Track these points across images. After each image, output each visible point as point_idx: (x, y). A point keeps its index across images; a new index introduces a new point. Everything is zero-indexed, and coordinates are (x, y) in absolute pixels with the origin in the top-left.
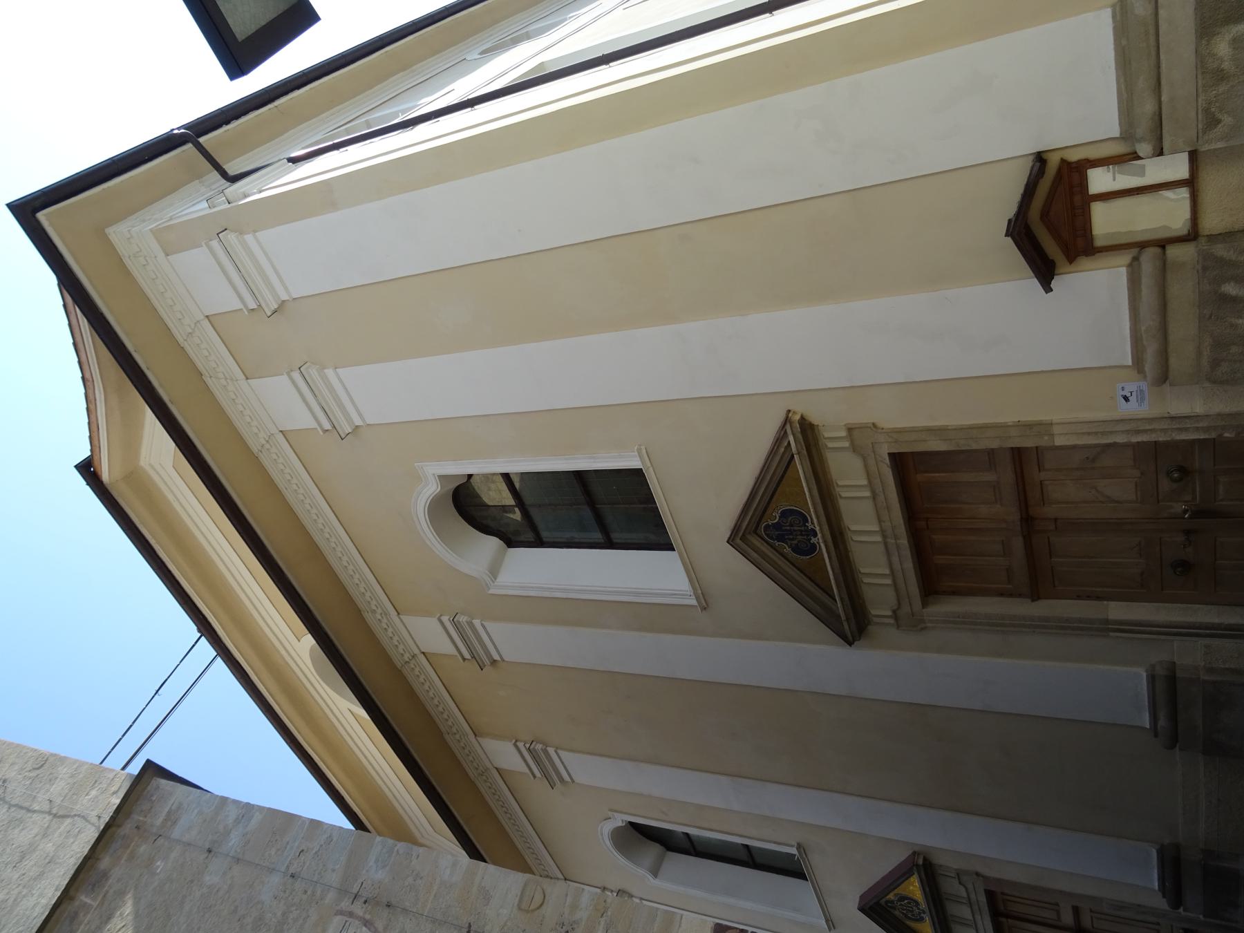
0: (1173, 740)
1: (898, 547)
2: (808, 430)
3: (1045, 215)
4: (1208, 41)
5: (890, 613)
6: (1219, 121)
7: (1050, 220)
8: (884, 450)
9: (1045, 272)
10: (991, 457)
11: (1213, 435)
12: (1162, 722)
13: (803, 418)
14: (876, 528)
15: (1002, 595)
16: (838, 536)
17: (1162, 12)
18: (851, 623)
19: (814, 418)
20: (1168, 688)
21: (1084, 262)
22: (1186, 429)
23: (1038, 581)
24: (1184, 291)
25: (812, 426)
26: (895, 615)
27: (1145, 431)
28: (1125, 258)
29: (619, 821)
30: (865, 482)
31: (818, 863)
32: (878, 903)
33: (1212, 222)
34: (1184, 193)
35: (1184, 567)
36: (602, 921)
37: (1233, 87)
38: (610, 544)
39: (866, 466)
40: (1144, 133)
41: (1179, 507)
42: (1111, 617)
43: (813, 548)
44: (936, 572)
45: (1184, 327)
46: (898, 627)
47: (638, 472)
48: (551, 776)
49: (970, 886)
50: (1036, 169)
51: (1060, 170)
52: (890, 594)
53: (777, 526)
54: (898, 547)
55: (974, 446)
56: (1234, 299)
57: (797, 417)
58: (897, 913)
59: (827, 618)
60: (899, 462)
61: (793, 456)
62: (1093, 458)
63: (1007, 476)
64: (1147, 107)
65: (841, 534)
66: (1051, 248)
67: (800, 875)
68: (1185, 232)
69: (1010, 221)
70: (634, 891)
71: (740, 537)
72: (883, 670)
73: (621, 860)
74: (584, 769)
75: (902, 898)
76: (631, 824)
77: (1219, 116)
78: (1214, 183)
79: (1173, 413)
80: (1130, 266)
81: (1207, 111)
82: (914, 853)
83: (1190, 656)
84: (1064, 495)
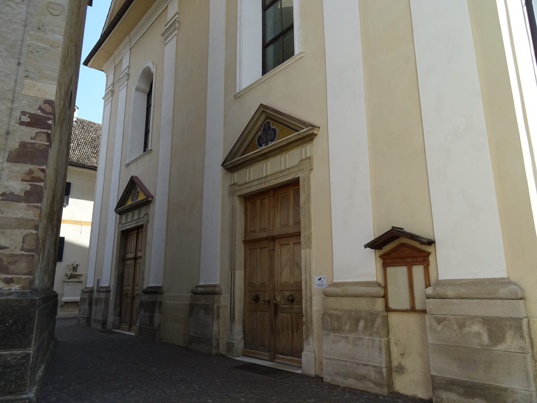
0: (195, 293)
1: (261, 183)
2: (310, 138)
3: (403, 245)
4: (480, 322)
5: (235, 182)
6: (439, 324)
7: (400, 248)
8: (300, 175)
9: (375, 245)
10: (298, 223)
11: (304, 313)
12: (200, 289)
13: (316, 135)
14: (268, 174)
15: (245, 229)
16: (265, 156)
17: (500, 301)
18: (232, 165)
19: (316, 141)
20: (211, 292)
21: (380, 262)
22: (306, 303)
23: (251, 243)
24: (362, 305)
25: (312, 140)
26: (235, 184)
27: (306, 287)
28: (381, 280)
29: (153, 70)
30: (287, 167)
31: (147, 157)
32: (135, 184)
33: (393, 318)
34: (407, 306)
35: (256, 299)
36: (48, 46)
37: (456, 331)
38: (265, 46)
39: (294, 167)
40: (442, 292)
41: (278, 298)
42: (236, 271)
43: (261, 146)
44: (253, 200)
45: (347, 304)
46: (230, 186)
47: (292, 54)
48: (166, 34)
49: (144, 219)
50: (424, 240)
51: (425, 252)
52: (243, 182)
53: (269, 127)
54: (261, 183)
55: (301, 215)
56: (357, 325)
57: (316, 132)
58: (133, 191)
59: (232, 155)
60: (296, 182)
61: (298, 131)
62: (296, 264)
63: (291, 230)
64: (450, 293)
65: (266, 158)
66: (387, 248)
67: (145, 150)
68: (390, 306)
69: (402, 229)
70: (130, 80)
71: (263, 109)
72: (215, 182)
73: (139, 73)
74: (170, 49)
75: (138, 193)
76: (153, 74)
77: (442, 324)
78: (412, 319)
79: (313, 298)
80: (377, 282)
81: (445, 319)
82: (153, 197)
83: (224, 300)
84: (283, 254)
